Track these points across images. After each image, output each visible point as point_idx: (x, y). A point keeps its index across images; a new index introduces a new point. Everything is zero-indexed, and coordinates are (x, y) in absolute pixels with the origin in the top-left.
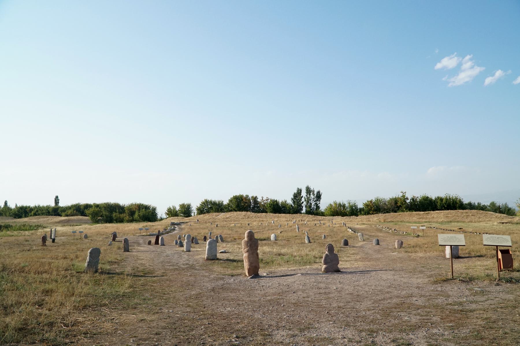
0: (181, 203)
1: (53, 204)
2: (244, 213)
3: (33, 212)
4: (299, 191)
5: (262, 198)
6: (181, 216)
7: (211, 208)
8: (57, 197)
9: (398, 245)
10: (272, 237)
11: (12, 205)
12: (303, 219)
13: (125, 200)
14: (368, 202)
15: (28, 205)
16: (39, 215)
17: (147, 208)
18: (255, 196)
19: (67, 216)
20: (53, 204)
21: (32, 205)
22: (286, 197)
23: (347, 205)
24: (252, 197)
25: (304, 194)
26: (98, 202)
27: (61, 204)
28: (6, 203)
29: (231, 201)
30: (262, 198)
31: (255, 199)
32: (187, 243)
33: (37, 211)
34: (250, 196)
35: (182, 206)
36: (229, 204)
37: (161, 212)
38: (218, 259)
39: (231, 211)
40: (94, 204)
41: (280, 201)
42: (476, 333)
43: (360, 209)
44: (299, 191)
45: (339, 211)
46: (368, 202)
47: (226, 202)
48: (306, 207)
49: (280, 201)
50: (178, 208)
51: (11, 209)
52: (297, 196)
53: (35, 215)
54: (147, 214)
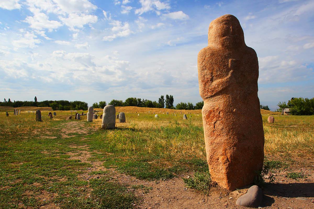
0: (100, 101)
1: (34, 101)
2: (134, 107)
3: (23, 104)
4: (162, 97)
5: (143, 99)
6: (100, 108)
7: (116, 104)
8: (36, 97)
9: (271, 120)
10: (156, 116)
11: (12, 101)
12: (165, 111)
13: (71, 99)
14: (198, 103)
15: (21, 101)
16: (27, 106)
17: (82, 103)
18: (139, 98)
19: (41, 107)
20: (34, 101)
21: (23, 101)
22: (155, 99)
23: (187, 104)
24: (138, 99)
25: (165, 98)
26: (57, 100)
27: (38, 101)
28: (9, 100)
29: (126, 101)
30: (143, 99)
31: (139, 100)
32: (89, 115)
33: (26, 104)
34: (137, 98)
35: (101, 103)
36: (125, 103)
37: (90, 105)
38: (116, 128)
39: (127, 106)
40: (55, 101)
41: (153, 102)
42: (190, 153)
43: (194, 107)
44: (162, 97)
45: (182, 107)
46: (198, 103)
47: (124, 101)
48: (166, 105)
49: (153, 102)
50: (99, 104)
51: (12, 103)
52: (161, 99)
53: (24, 106)
54: (82, 106)
